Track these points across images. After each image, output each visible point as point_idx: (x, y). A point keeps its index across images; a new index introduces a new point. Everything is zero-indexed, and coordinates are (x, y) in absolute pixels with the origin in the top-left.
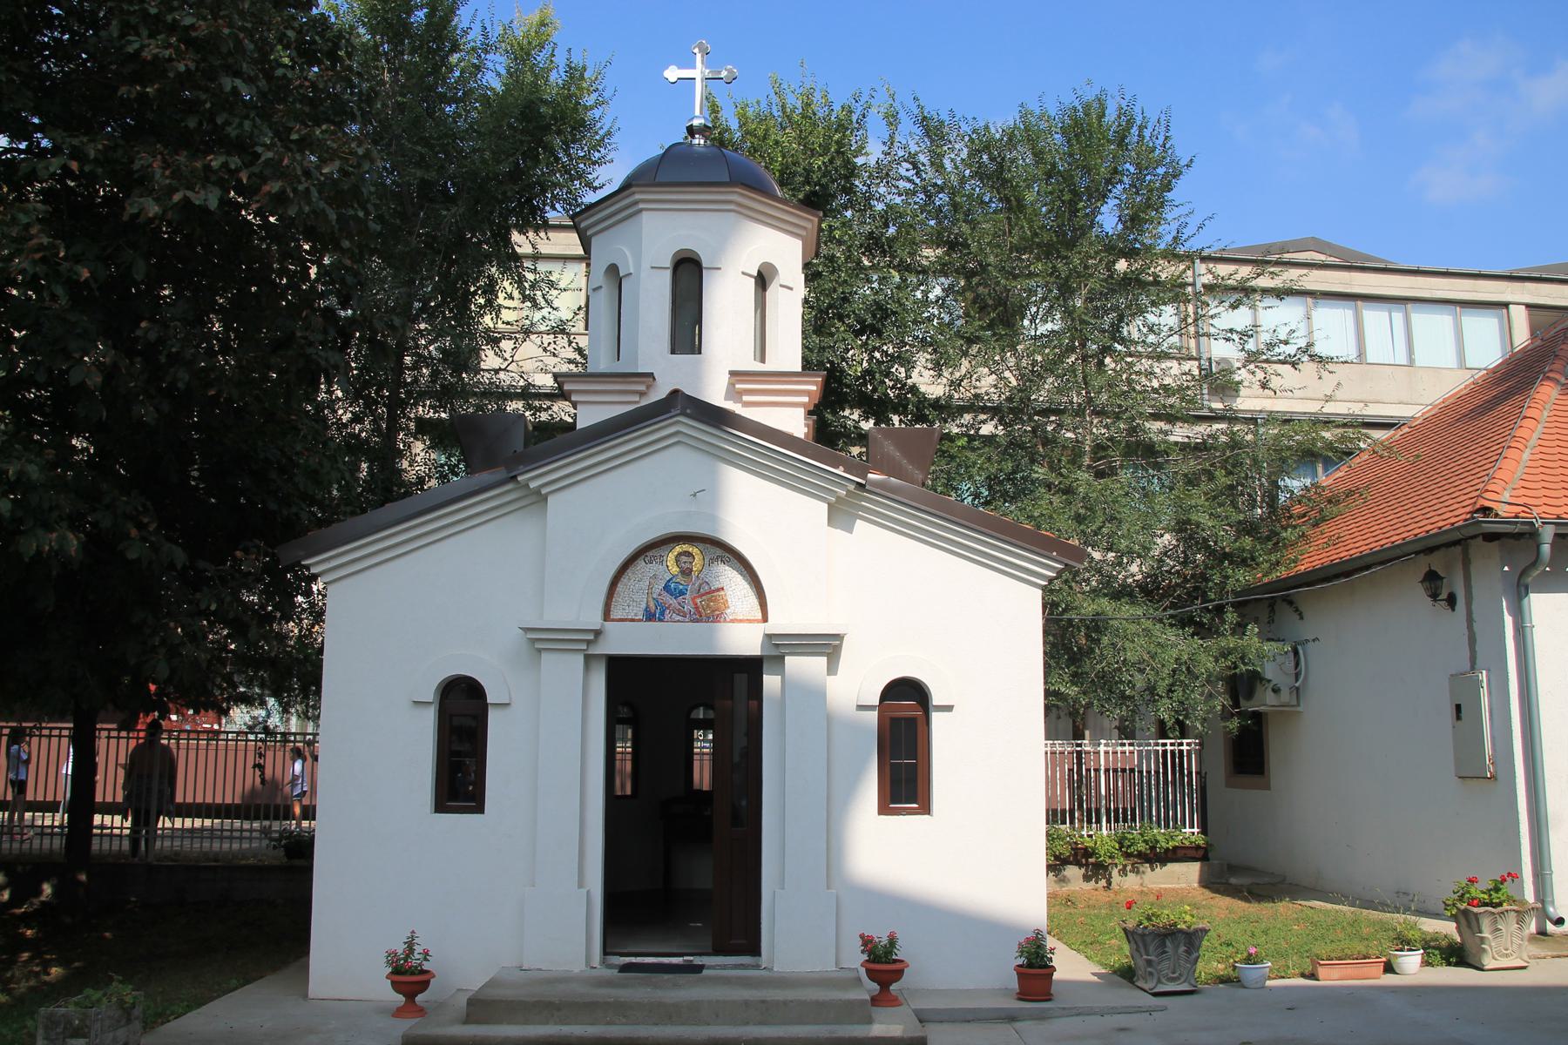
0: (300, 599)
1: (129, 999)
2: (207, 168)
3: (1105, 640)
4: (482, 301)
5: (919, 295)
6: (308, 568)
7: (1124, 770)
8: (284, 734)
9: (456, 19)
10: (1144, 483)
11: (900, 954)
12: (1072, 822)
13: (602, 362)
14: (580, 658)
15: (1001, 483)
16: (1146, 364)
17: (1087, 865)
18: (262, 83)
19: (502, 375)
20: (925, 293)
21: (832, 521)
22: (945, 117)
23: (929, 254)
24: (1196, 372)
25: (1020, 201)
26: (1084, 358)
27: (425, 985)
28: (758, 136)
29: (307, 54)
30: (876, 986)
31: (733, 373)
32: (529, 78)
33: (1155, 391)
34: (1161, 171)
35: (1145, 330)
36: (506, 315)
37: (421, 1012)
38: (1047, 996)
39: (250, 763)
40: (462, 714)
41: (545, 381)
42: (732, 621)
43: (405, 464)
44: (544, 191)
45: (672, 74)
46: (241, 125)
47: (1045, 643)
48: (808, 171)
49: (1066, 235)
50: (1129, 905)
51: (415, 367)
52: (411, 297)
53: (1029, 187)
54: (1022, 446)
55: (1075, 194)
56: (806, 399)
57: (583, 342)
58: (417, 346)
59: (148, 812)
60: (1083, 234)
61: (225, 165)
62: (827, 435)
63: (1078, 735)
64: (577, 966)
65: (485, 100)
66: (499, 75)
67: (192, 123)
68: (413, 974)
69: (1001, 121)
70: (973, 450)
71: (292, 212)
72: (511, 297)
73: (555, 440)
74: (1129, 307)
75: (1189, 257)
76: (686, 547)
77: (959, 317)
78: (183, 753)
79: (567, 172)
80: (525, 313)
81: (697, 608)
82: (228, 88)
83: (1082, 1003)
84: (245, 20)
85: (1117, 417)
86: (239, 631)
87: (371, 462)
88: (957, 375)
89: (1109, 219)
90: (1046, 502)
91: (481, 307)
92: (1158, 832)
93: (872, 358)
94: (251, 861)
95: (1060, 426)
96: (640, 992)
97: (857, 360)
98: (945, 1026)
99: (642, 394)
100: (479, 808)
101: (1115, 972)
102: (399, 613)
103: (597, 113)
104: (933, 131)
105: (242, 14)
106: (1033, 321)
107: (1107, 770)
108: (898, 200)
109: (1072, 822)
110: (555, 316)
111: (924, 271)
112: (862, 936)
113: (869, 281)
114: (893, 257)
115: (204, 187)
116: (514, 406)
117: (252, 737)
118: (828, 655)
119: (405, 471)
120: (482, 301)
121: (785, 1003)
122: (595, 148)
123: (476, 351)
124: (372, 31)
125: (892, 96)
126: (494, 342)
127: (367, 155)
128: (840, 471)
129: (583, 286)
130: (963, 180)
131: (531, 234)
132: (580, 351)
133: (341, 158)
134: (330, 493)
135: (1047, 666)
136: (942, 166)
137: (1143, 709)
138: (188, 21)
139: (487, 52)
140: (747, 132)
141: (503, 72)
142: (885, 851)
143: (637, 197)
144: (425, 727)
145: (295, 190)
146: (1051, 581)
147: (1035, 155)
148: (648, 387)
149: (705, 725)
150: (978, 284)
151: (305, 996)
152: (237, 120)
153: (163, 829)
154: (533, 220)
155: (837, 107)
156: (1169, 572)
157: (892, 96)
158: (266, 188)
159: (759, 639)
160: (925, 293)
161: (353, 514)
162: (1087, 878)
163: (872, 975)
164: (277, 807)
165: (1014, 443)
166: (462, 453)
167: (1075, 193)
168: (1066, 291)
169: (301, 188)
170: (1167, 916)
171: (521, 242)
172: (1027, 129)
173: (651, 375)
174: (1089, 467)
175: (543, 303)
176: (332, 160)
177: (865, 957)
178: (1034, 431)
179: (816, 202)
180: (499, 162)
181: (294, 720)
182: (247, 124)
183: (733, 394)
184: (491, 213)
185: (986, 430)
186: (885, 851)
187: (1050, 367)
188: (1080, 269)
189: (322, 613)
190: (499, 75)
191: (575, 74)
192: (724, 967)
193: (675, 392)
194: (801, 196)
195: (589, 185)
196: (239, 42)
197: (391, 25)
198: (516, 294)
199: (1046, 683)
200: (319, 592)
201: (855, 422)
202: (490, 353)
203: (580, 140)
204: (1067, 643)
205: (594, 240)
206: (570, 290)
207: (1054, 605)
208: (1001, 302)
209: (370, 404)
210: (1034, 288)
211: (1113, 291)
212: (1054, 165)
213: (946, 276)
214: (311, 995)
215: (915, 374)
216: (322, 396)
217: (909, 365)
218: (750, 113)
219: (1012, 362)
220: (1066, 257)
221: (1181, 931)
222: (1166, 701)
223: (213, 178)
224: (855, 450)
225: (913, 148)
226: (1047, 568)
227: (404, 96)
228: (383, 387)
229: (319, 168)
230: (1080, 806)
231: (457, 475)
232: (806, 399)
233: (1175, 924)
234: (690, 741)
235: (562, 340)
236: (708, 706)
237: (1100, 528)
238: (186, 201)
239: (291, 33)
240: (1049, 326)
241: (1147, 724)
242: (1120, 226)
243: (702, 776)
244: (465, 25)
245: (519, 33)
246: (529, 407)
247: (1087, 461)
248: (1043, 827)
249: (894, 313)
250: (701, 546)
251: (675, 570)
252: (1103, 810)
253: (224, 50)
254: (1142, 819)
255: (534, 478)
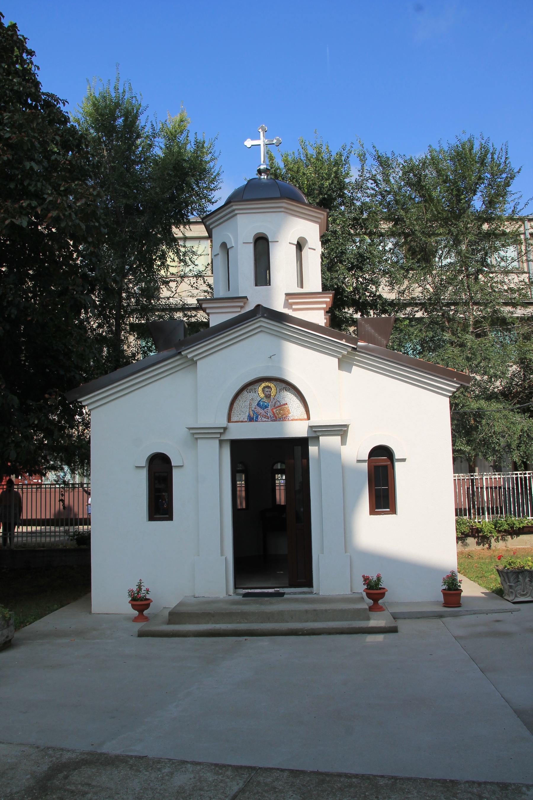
0: (77, 417)
1: (8, 616)
2: (21, 207)
3: (484, 422)
4: (159, 263)
5: (381, 248)
6: (81, 402)
7: (496, 488)
8: (73, 484)
9: (138, 122)
10: (501, 339)
11: (383, 585)
12: (470, 515)
13: (221, 293)
14: (217, 442)
15: (427, 343)
16: (500, 277)
17: (478, 537)
18: (45, 164)
19: (171, 300)
20: (384, 247)
21: (340, 367)
22: (389, 155)
23: (385, 226)
24: (527, 280)
25: (430, 196)
26: (468, 276)
27: (147, 606)
28: (294, 174)
29: (66, 146)
30: (371, 602)
31: (287, 295)
32: (176, 149)
33: (506, 291)
34: (504, 176)
35: (499, 260)
36: (172, 270)
37: (146, 619)
38: (459, 605)
39: (57, 499)
40: (160, 472)
41: (193, 301)
42: (292, 420)
43: (125, 347)
44: (187, 206)
45: (249, 143)
46: (36, 185)
47: (452, 425)
48: (321, 187)
49: (454, 214)
50: (499, 558)
51: (128, 298)
52: (124, 264)
53: (435, 188)
54: (437, 323)
55: (459, 193)
56: (325, 306)
57: (211, 281)
58: (128, 288)
59: (10, 524)
60: (464, 212)
61: (29, 205)
62: (336, 322)
63: (472, 470)
64: (222, 595)
65: (156, 162)
66: (161, 148)
67: (12, 186)
68: (141, 600)
69: (419, 154)
70: (412, 326)
71: (63, 225)
72: (174, 261)
73: (199, 332)
74: (490, 248)
75: (522, 220)
76: (267, 384)
77: (402, 258)
78: (25, 495)
79: (198, 195)
80: (181, 269)
81: (274, 414)
82: (28, 168)
83: (476, 608)
84: (35, 132)
85: (486, 305)
86: (49, 434)
87: (108, 346)
88: (402, 288)
89: (478, 203)
90: (452, 351)
91: (159, 266)
92: (514, 519)
93: (357, 281)
94: (61, 547)
95: (456, 311)
96: (253, 607)
97: (350, 283)
98: (407, 621)
99: (242, 307)
100: (171, 518)
101: (493, 592)
102: (127, 422)
103: (212, 164)
104: (384, 163)
105: (33, 130)
106: (440, 258)
107: (487, 488)
108: (368, 200)
109: (470, 515)
110: (196, 269)
111: (382, 235)
112: (363, 576)
113: (355, 242)
114: (366, 229)
115: (20, 217)
116: (178, 315)
117: (57, 486)
118: (341, 435)
119: (126, 351)
120: (159, 263)
121: (326, 611)
122: (212, 182)
123: (158, 289)
124: (97, 130)
125: (362, 145)
126: (166, 283)
127: (99, 195)
128: (343, 342)
129: (210, 253)
130: (400, 188)
131: (182, 227)
132: (209, 286)
133: (85, 197)
134: (89, 364)
135: (453, 436)
136: (389, 181)
137: (505, 456)
138: (7, 135)
139: (154, 137)
140: (289, 169)
141: (163, 147)
142: (372, 532)
143: (234, 207)
144: (142, 480)
145: (64, 215)
146: (454, 393)
147: (437, 172)
148: (245, 304)
149: (281, 472)
150: (411, 241)
151: (90, 612)
152: (34, 183)
153: (18, 532)
154: (182, 220)
155: (334, 154)
156: (516, 385)
157: (362, 145)
158: (50, 215)
159: (306, 429)
160: (384, 247)
161: (101, 374)
162: (478, 544)
163: (369, 595)
164: (72, 519)
165: (433, 322)
166: (153, 340)
167: (458, 190)
168: (457, 242)
169: (67, 213)
170: (519, 563)
171: (177, 232)
172: (432, 159)
173: (246, 298)
174: (472, 332)
175: (190, 263)
176: (81, 199)
177: (365, 587)
178: (443, 315)
179: (326, 204)
180: (164, 193)
181: (77, 477)
182: (39, 185)
183: (287, 305)
184: (161, 219)
185: (419, 315)
186: (372, 532)
187: (450, 281)
188: (464, 230)
189: (89, 423)
190: (161, 148)
191: (200, 146)
192: (295, 593)
193: (258, 306)
194: (318, 201)
195: (210, 201)
196: (32, 144)
197: (106, 127)
198: (176, 259)
199: (453, 445)
200: (87, 413)
201: (351, 316)
202: (165, 289)
203: (204, 179)
204: (464, 425)
205: (213, 230)
206: (203, 254)
207: (457, 405)
208: (423, 249)
209: (106, 317)
210: (441, 241)
211: (481, 240)
212: (447, 176)
213: (394, 237)
214: (93, 612)
215: (380, 289)
216: (83, 316)
217: (377, 284)
218: (290, 159)
219: (430, 279)
220: (456, 224)
221: (527, 570)
222: (516, 452)
223: (24, 212)
224: (352, 329)
225: (374, 173)
226: (452, 387)
227: (114, 162)
228: (113, 306)
229: (75, 203)
230: (474, 507)
231: (151, 351)
232: (325, 306)
233: (523, 567)
234: (274, 480)
235: (200, 281)
236: (282, 462)
237: (479, 363)
238: (12, 224)
239: (58, 138)
240: (449, 260)
241: (507, 464)
242: (484, 207)
243: (281, 497)
244: (143, 124)
245: (170, 126)
246: (185, 315)
247: (471, 329)
248: (453, 518)
249: (368, 258)
250: (275, 383)
251: (262, 395)
252: (486, 509)
253: (25, 148)
254: (506, 513)
255: (190, 353)
